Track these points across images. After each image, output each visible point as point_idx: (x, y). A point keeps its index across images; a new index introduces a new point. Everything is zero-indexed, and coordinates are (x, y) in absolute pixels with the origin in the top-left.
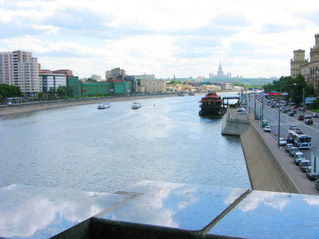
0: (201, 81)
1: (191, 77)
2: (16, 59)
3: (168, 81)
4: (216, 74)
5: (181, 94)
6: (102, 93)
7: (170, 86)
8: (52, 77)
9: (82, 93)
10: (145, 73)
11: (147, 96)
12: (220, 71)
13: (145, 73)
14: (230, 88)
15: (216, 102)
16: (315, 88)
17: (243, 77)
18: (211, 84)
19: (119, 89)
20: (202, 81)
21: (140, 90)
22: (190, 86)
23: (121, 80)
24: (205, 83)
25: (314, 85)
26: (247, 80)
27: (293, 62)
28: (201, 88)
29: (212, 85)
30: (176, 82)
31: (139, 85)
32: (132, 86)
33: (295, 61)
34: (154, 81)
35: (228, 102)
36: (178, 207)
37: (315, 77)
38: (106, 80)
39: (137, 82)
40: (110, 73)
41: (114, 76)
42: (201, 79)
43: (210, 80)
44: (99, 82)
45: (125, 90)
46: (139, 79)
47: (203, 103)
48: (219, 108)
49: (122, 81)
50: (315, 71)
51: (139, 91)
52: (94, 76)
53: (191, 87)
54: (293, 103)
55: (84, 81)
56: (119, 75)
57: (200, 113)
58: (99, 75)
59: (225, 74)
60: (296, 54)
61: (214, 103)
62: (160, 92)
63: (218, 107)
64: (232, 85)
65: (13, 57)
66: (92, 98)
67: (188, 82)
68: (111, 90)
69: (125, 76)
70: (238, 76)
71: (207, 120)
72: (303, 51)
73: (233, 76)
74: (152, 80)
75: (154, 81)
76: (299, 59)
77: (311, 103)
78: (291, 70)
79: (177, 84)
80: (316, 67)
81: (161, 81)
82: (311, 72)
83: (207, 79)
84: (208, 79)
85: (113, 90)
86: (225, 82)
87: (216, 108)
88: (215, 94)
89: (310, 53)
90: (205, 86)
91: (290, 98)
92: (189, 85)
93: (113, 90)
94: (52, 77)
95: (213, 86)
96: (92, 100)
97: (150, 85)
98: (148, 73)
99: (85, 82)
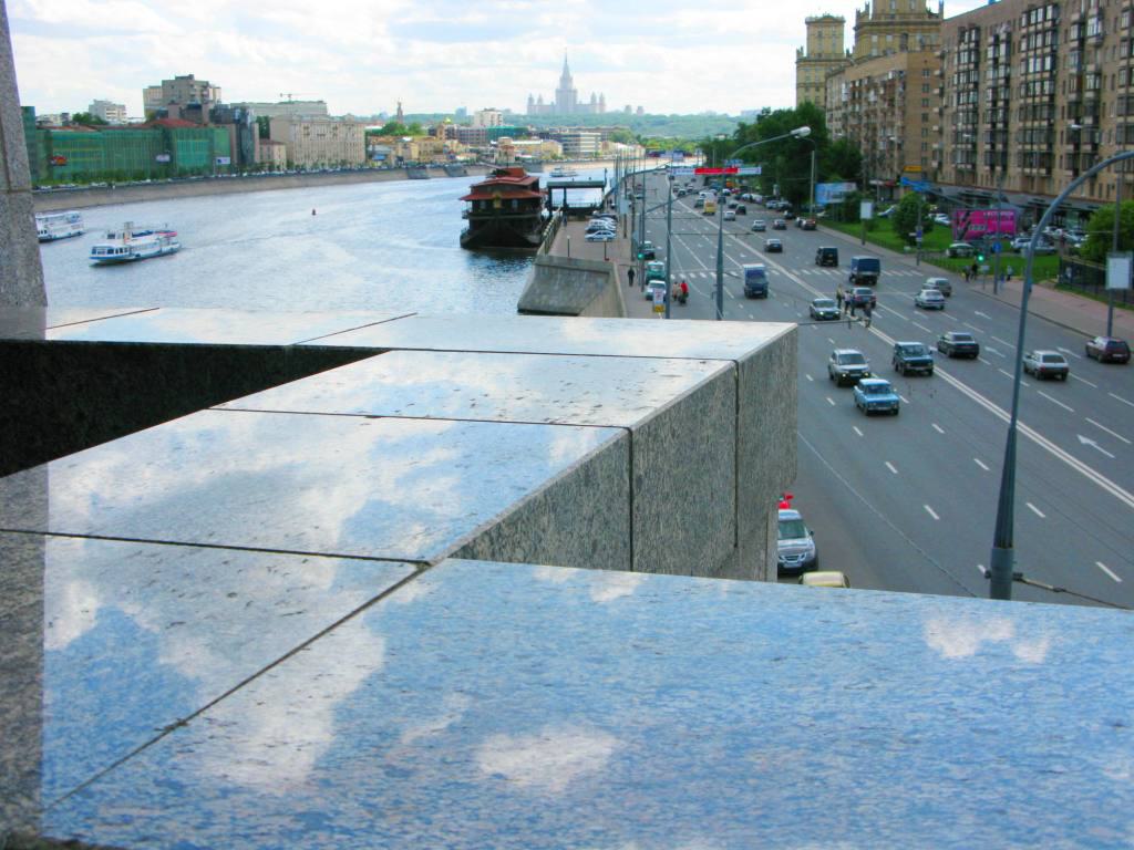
0: (492, 124)
1: (461, 112)
3: (375, 124)
4: (550, 98)
5: (415, 170)
6: (124, 168)
7: (379, 144)
9: (50, 167)
10: (290, 96)
11: (293, 181)
12: (566, 90)
13: (290, 96)
14: (597, 148)
15: (518, 200)
16: (865, 150)
17: (647, 111)
18: (529, 135)
19: (189, 152)
20: (495, 126)
21: (269, 156)
22: (453, 144)
23: (201, 123)
24: (507, 132)
25: (863, 140)
26: (660, 121)
27: (805, 60)
28: (492, 151)
29: (530, 139)
30: (402, 128)
31: (267, 140)
32: (240, 145)
33: (813, 57)
34: (321, 123)
35: (565, 200)
37: (866, 112)
38: (144, 120)
39: (256, 126)
40: (159, 95)
41: (172, 107)
42: (492, 117)
43: (528, 119)
44: (113, 128)
45: (212, 156)
46: (266, 118)
47: (476, 204)
48: (529, 220)
49: (200, 124)
50: (864, 91)
51: (265, 159)
52: (98, 104)
53: (457, 147)
54: (782, 203)
55: (59, 123)
56: (189, 102)
57: (467, 239)
58: (117, 103)
59: (583, 98)
60: (816, 31)
61: (515, 204)
62: (344, 163)
63: (526, 216)
64: (603, 140)
66: (86, 186)
67: (446, 127)
68: (160, 158)
69: (211, 106)
70: (628, 108)
71: (485, 261)
72: (839, 22)
74: (312, 122)
75: (321, 123)
76: (826, 47)
77: (838, 201)
78: (799, 86)
79: (406, 135)
80: (869, 78)
81: (348, 122)
82: (854, 94)
83: (518, 116)
84: (524, 117)
85: (167, 158)
86: (579, 129)
87: (521, 220)
88: (519, 173)
89: (855, 29)
90: (506, 143)
91: (775, 186)
92: (449, 138)
93: (167, 158)
95: (535, 142)
96: (86, 193)
97: (305, 141)
98: (304, 93)
99: (60, 128)
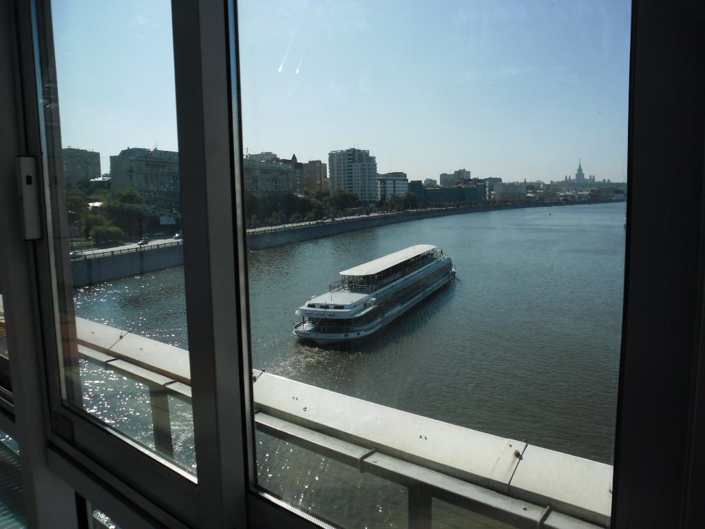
2: (350, 159)
4: (573, 177)
8: (392, 182)
36: (435, 311)
59: (587, 177)
70: (604, 180)
73: (597, 180)
94: (392, 182)
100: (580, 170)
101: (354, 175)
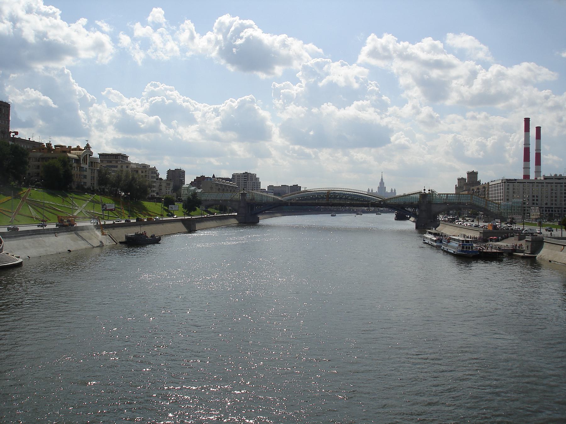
2: (245, 178)
4: (375, 190)
59: (388, 190)
65: (243, 177)
73: (398, 194)
100: (382, 183)
101: (247, 186)
